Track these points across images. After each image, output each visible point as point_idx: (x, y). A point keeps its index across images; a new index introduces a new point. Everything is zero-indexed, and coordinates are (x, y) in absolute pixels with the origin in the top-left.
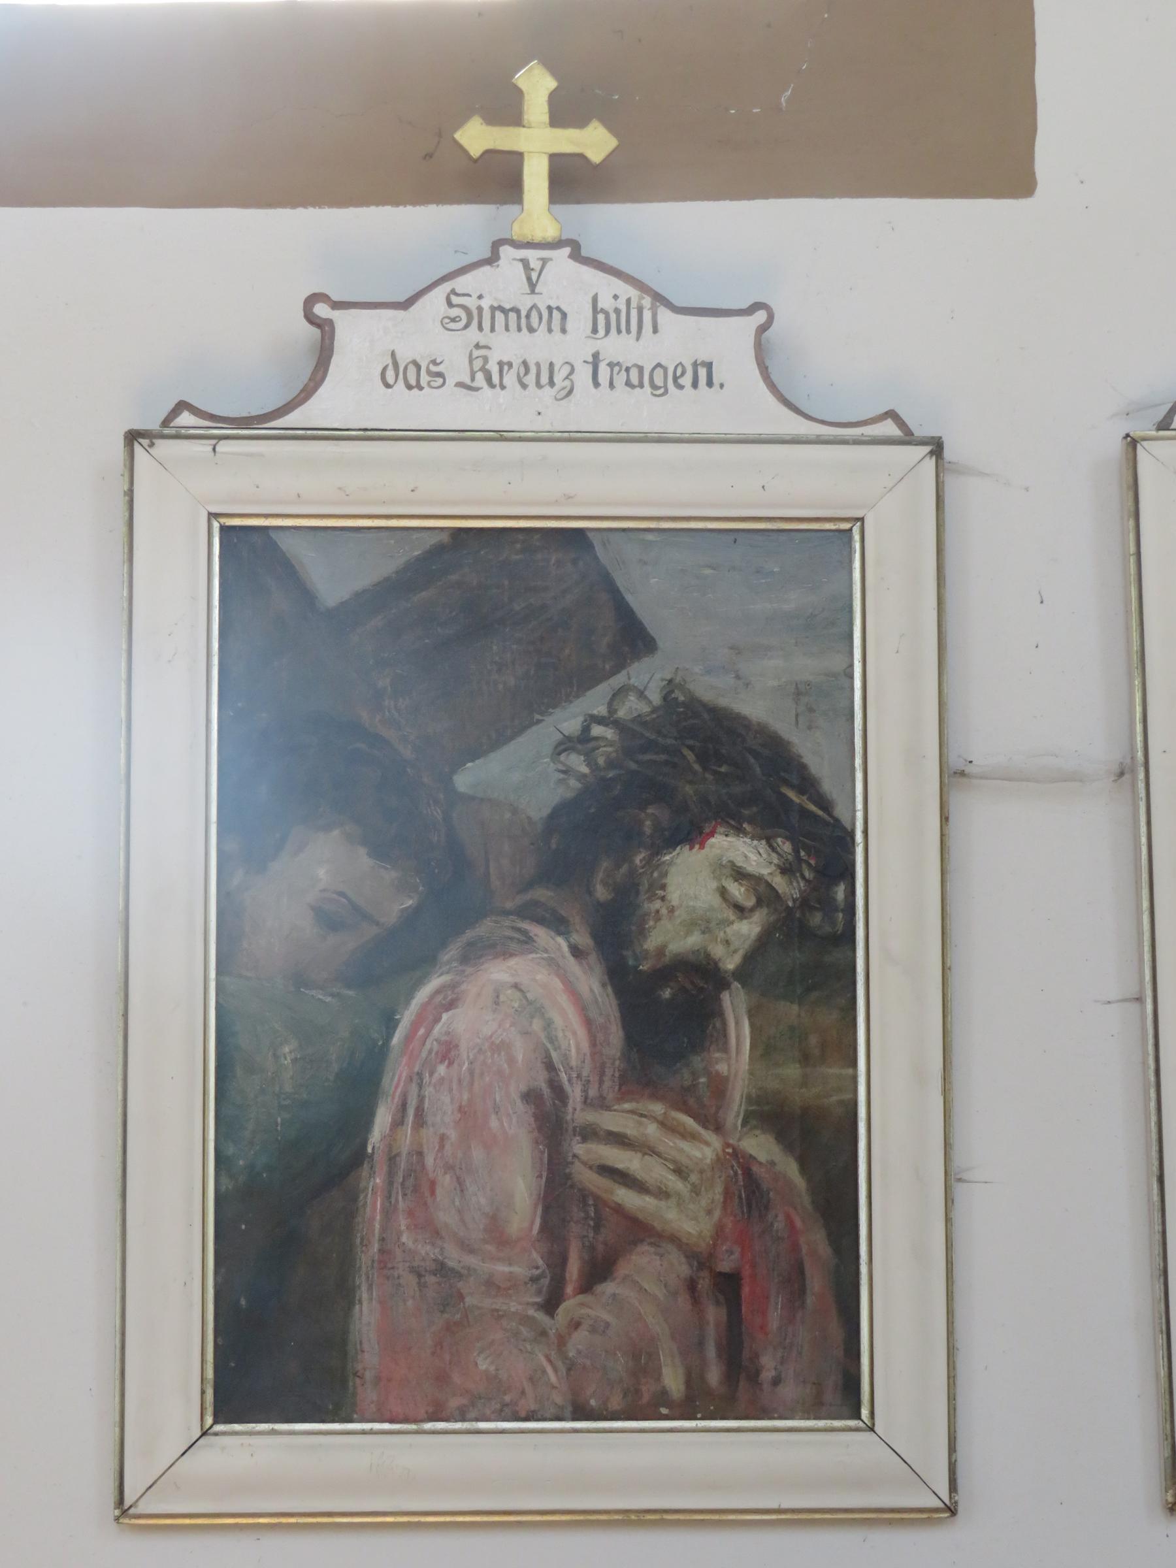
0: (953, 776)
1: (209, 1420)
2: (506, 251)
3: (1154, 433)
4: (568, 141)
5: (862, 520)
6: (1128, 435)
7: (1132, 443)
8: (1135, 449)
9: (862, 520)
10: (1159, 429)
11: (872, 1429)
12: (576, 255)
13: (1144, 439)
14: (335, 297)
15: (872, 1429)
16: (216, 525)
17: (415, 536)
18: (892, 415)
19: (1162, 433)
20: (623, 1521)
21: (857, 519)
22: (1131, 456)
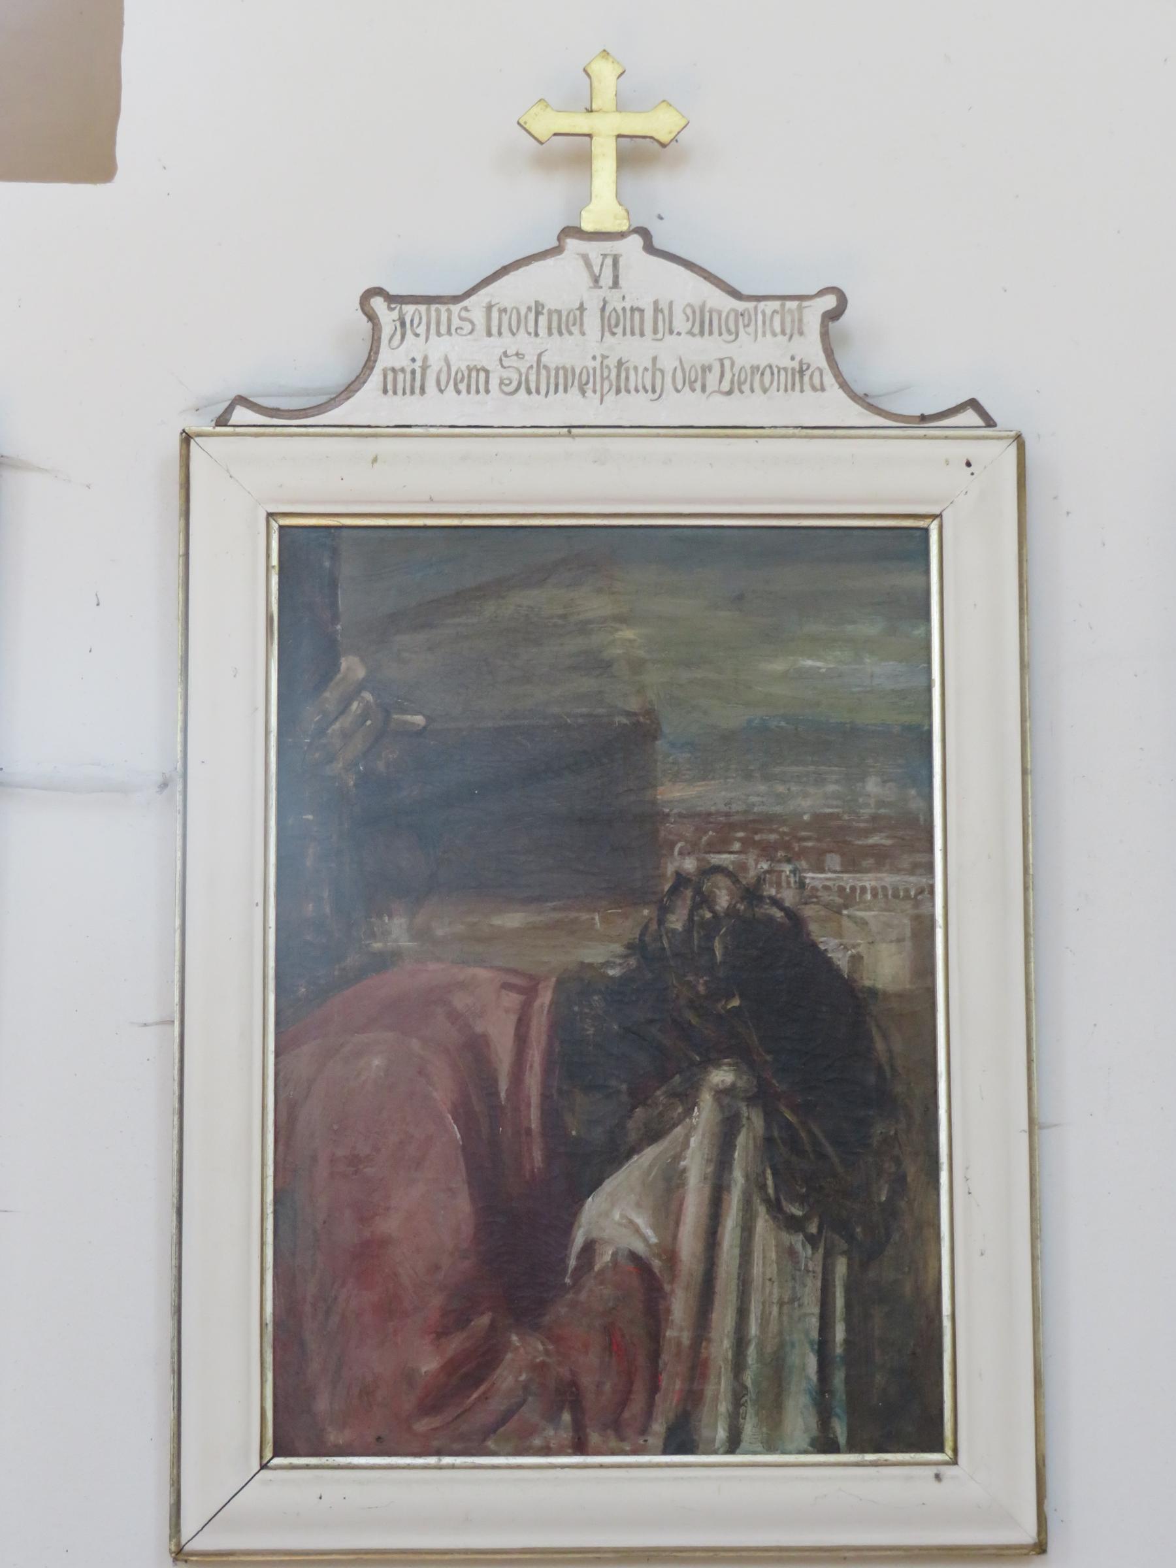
0: (175, 783)
1: (269, 1453)
2: (572, 244)
3: (211, 429)
4: (635, 124)
5: (940, 516)
6: (184, 431)
7: (187, 438)
8: (188, 445)
9: (940, 516)
10: (218, 425)
11: (263, 1467)
12: (650, 248)
13: (199, 435)
14: (393, 291)
15: (263, 1467)
16: (275, 526)
17: (855, 532)
18: (973, 404)
19: (219, 429)
20: (356, 1560)
21: (934, 517)
22: (184, 452)
